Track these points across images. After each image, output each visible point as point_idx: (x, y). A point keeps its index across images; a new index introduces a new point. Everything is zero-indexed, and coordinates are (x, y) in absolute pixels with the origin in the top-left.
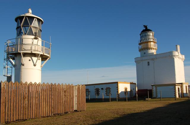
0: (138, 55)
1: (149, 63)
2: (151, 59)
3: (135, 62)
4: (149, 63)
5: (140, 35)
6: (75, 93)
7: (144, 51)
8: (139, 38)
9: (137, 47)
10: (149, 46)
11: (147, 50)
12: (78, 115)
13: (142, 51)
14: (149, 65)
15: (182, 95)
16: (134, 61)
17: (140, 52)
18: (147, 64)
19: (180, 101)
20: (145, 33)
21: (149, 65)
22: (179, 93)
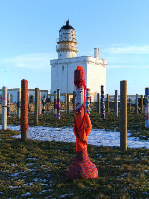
0: (55, 56)
1: (63, 66)
2: (65, 63)
3: (51, 64)
4: (63, 66)
5: (60, 31)
6: (128, 131)
7: (62, 53)
8: (57, 36)
9: (54, 45)
10: (70, 48)
11: (67, 51)
12: (62, 121)
13: (60, 52)
14: (63, 69)
15: (20, 130)
16: (50, 63)
17: (58, 52)
18: (61, 69)
19: (131, 49)
20: (66, 31)
21: (63, 69)
22: (39, 115)
